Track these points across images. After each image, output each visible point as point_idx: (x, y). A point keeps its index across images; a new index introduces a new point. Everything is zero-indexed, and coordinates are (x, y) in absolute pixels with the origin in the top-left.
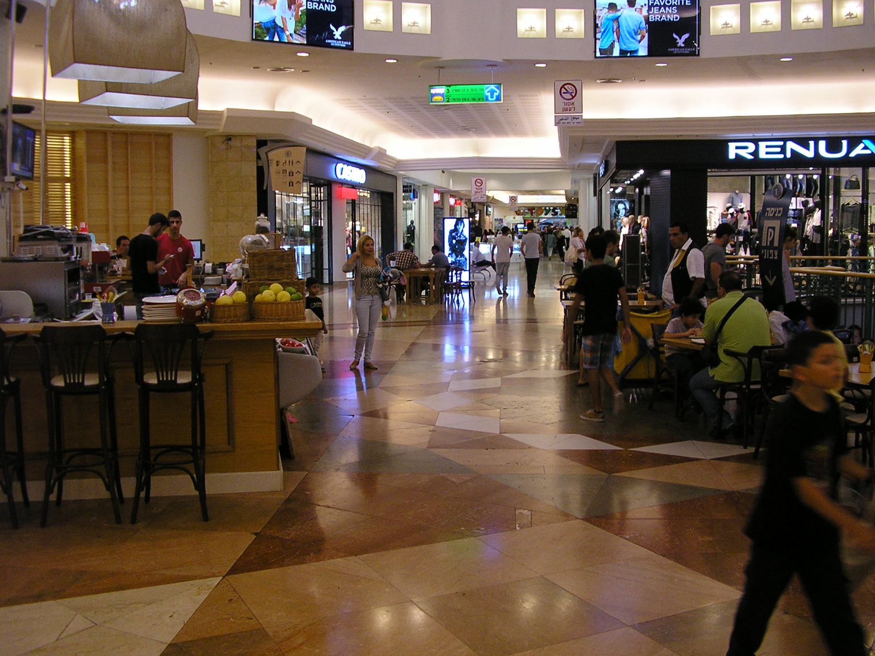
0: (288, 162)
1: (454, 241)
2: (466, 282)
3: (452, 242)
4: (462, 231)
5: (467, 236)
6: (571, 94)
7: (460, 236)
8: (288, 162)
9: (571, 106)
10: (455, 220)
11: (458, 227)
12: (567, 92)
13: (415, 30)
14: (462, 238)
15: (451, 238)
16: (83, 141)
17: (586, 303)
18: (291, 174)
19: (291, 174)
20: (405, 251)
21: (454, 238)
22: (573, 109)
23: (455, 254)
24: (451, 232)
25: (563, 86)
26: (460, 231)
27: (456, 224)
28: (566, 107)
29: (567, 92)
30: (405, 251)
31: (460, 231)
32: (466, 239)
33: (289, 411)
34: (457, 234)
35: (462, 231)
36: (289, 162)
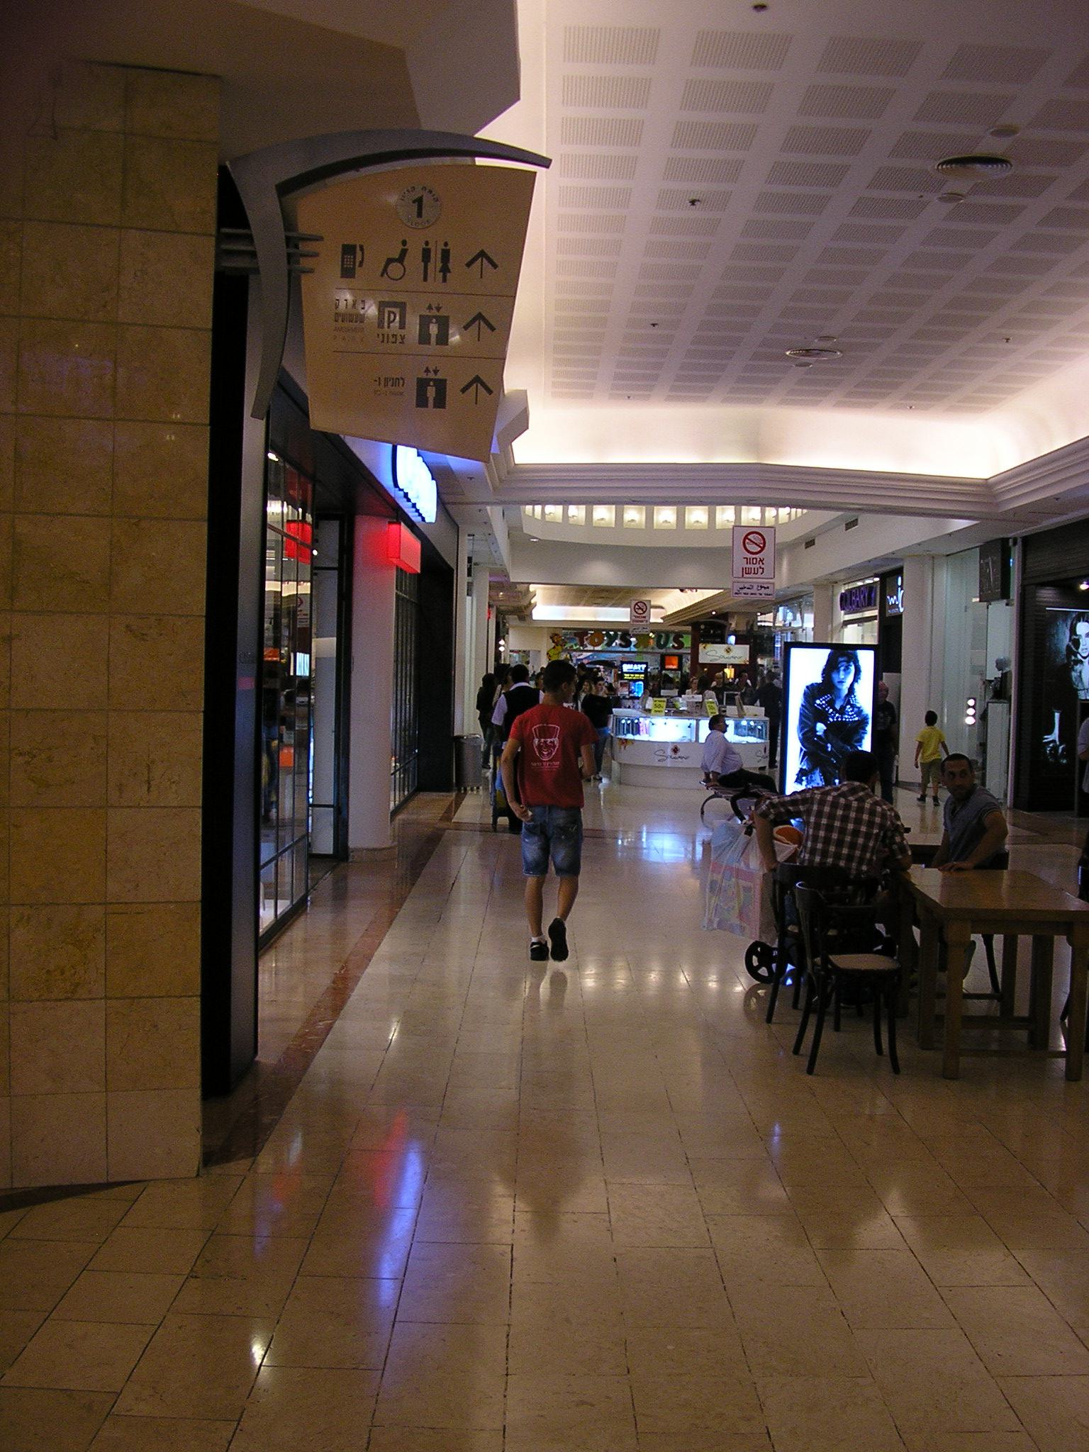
0: (414, 258)
1: (821, 727)
2: (283, 506)
3: (814, 730)
4: (851, 690)
5: (868, 709)
6: (642, 610)
7: (842, 711)
8: (414, 258)
9: (757, 566)
10: (825, 653)
11: (836, 678)
12: (640, 608)
13: (602, 524)
14: (850, 717)
15: (811, 714)
16: (338, 524)
17: (841, 868)
18: (431, 392)
19: (431, 392)
20: (853, 791)
21: (822, 717)
22: (761, 570)
23: (824, 774)
24: (812, 692)
25: (636, 604)
26: (845, 688)
27: (831, 668)
28: (749, 566)
29: (640, 608)
30: (853, 791)
31: (845, 688)
32: (863, 721)
33: (352, 852)
34: (831, 703)
35: (851, 690)
36: (426, 255)
